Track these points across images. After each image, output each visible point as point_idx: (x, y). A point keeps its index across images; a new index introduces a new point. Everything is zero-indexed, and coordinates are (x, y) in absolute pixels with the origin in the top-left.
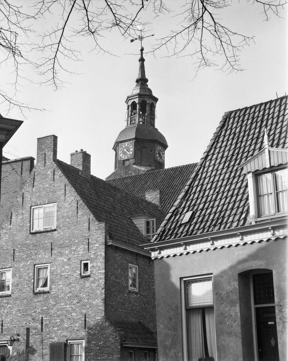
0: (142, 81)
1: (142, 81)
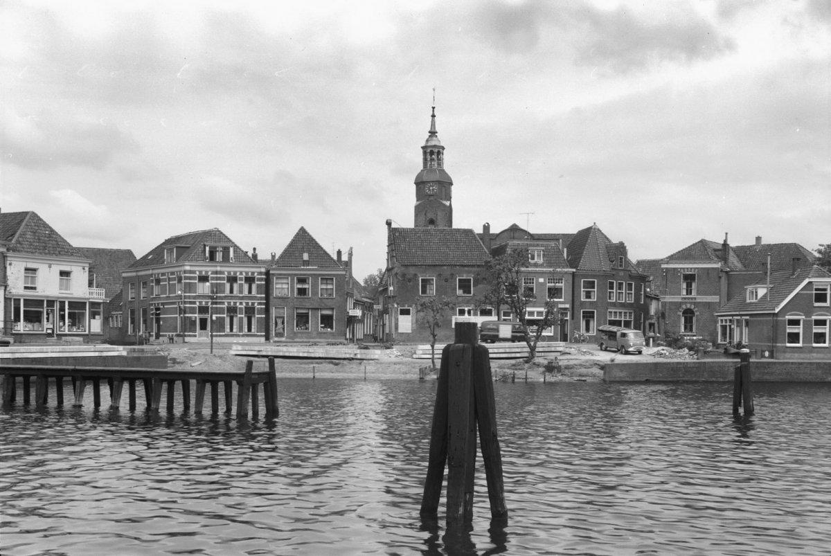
0: (433, 133)
1: (433, 133)
